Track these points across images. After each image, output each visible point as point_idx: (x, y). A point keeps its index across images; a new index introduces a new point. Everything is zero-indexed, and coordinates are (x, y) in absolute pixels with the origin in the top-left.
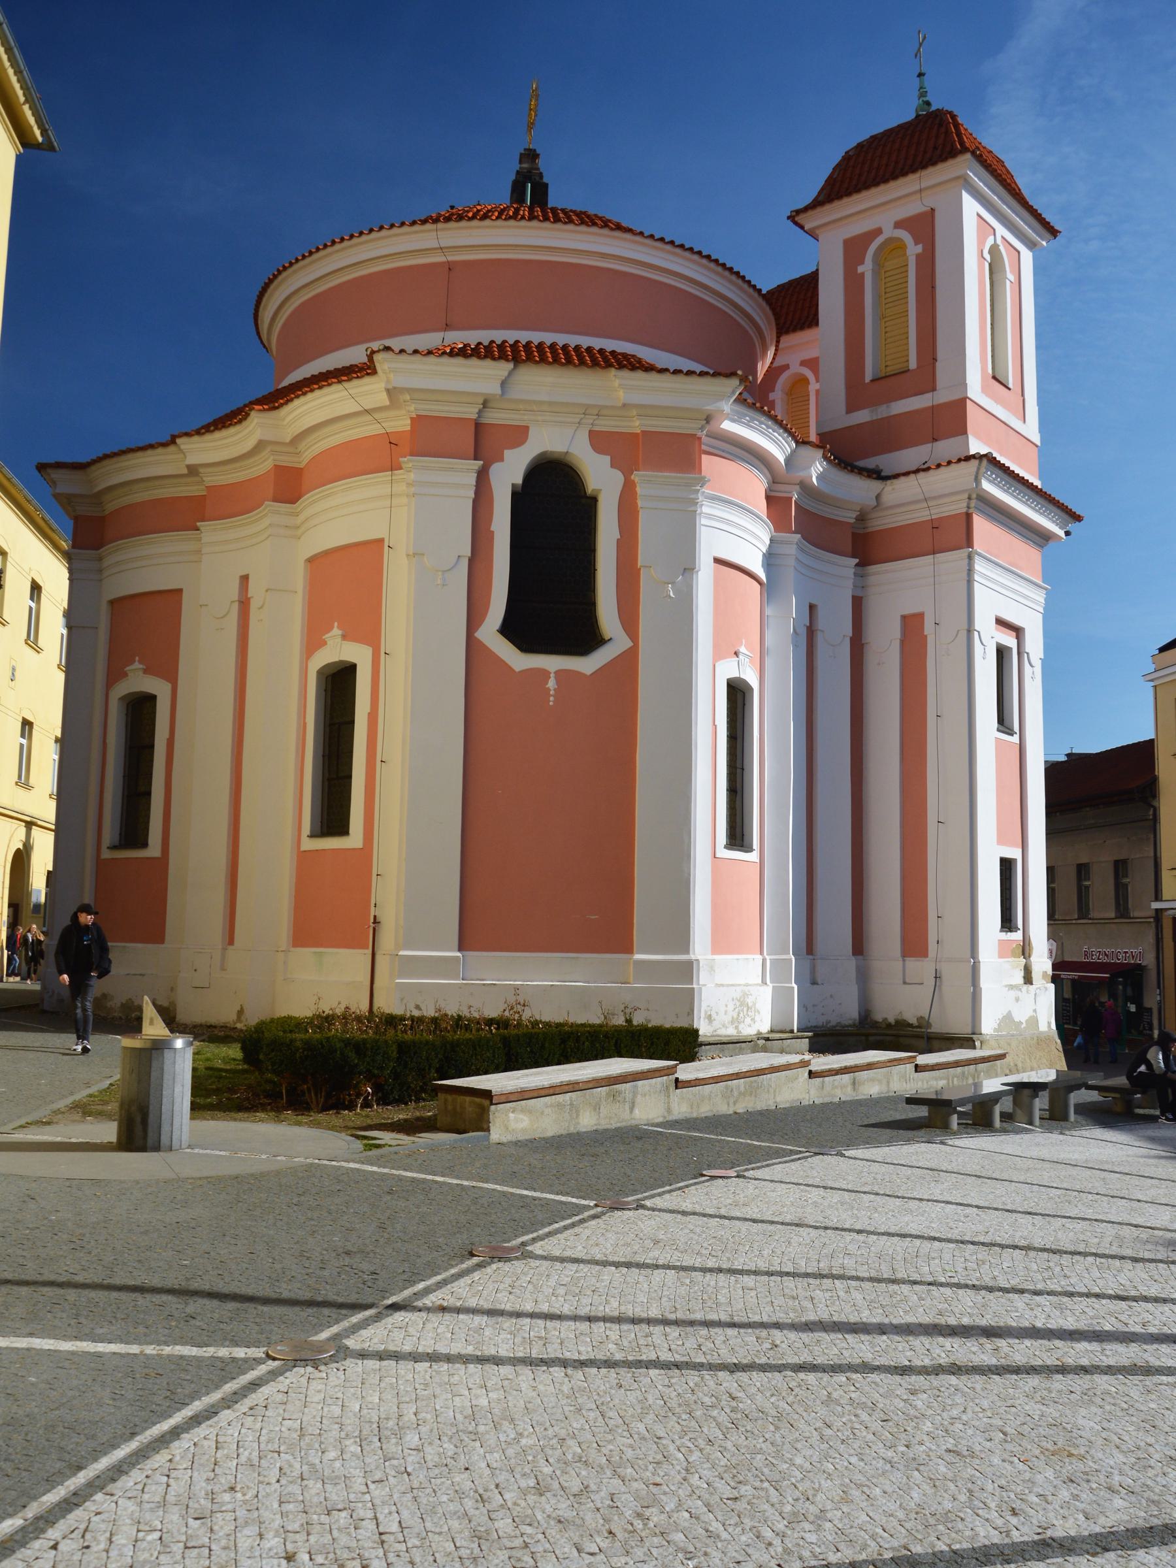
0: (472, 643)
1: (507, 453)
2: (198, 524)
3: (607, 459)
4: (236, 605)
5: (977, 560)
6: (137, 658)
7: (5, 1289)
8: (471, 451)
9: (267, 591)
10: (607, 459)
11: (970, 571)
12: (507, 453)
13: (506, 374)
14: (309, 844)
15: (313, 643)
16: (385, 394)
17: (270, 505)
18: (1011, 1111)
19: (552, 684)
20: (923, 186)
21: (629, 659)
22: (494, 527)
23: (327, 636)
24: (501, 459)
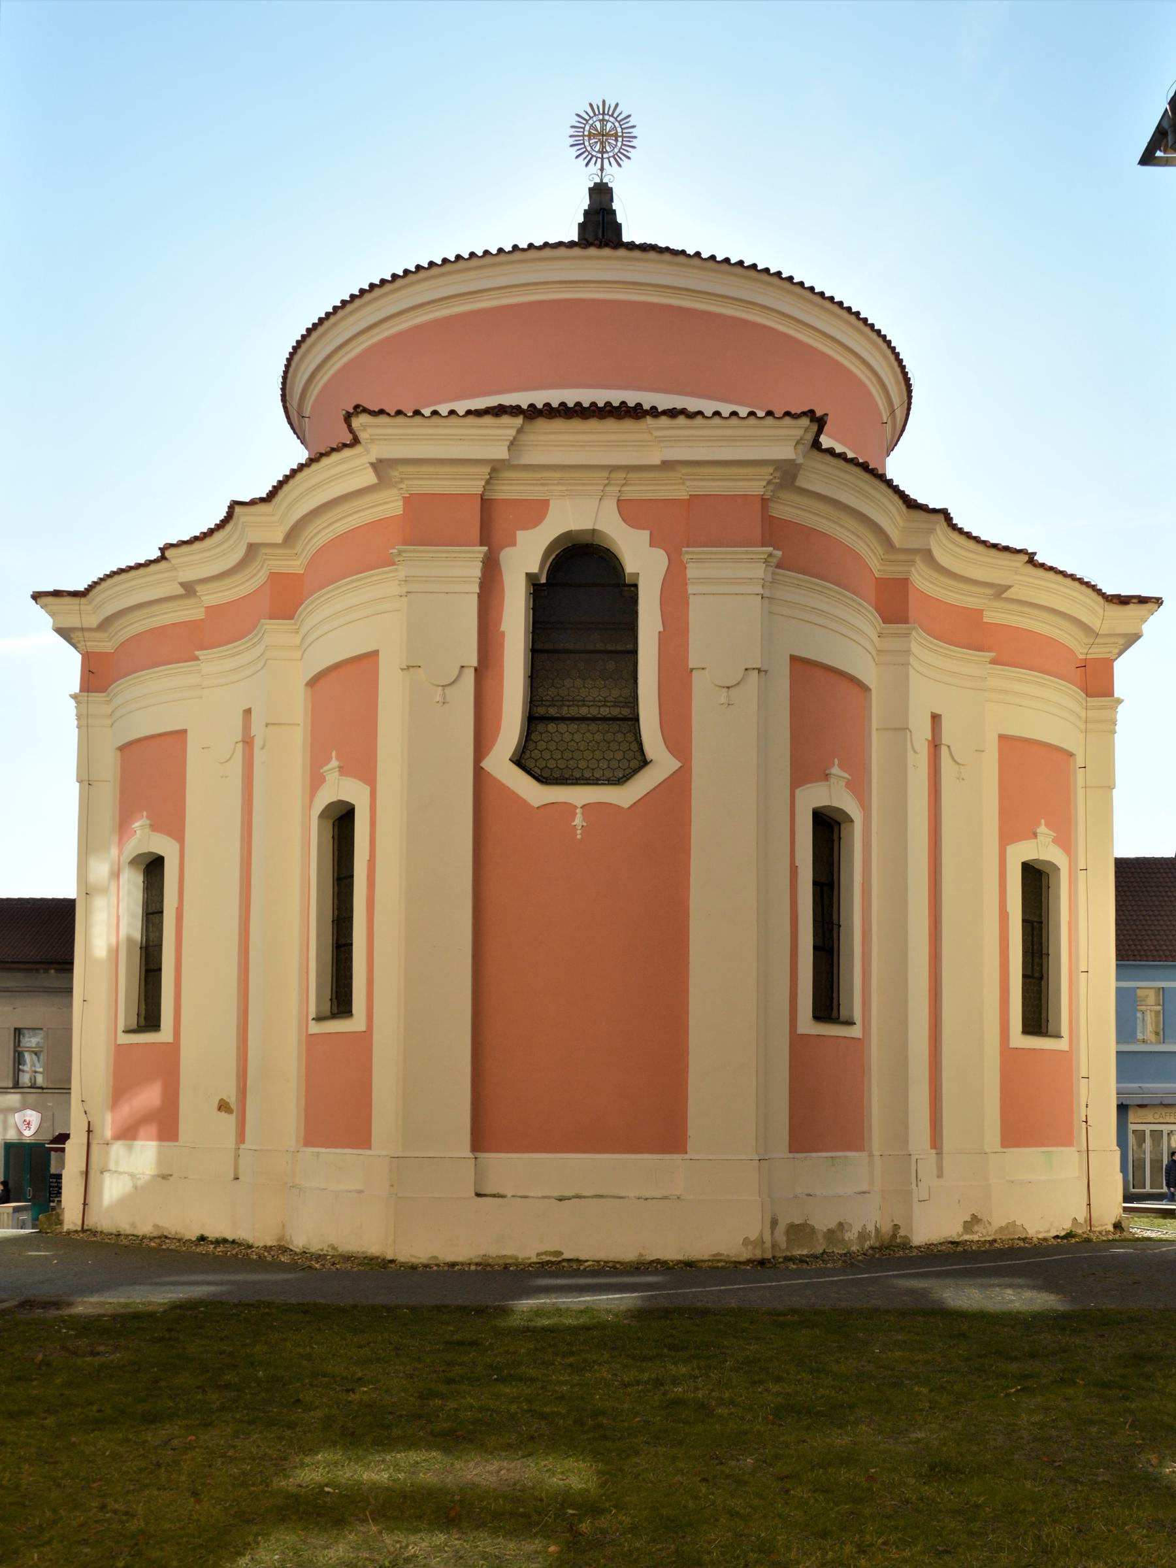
0: (479, 774)
1: (521, 535)
2: (197, 653)
3: (645, 534)
4: (240, 745)
8: (476, 534)
9: (267, 725)
10: (645, 534)
12: (521, 535)
13: (513, 432)
14: (315, 1028)
15: (316, 781)
16: (370, 470)
17: (269, 625)
18: (507, 457)
19: (578, 821)
21: (678, 784)
22: (504, 627)
23: (325, 769)
24: (513, 543)
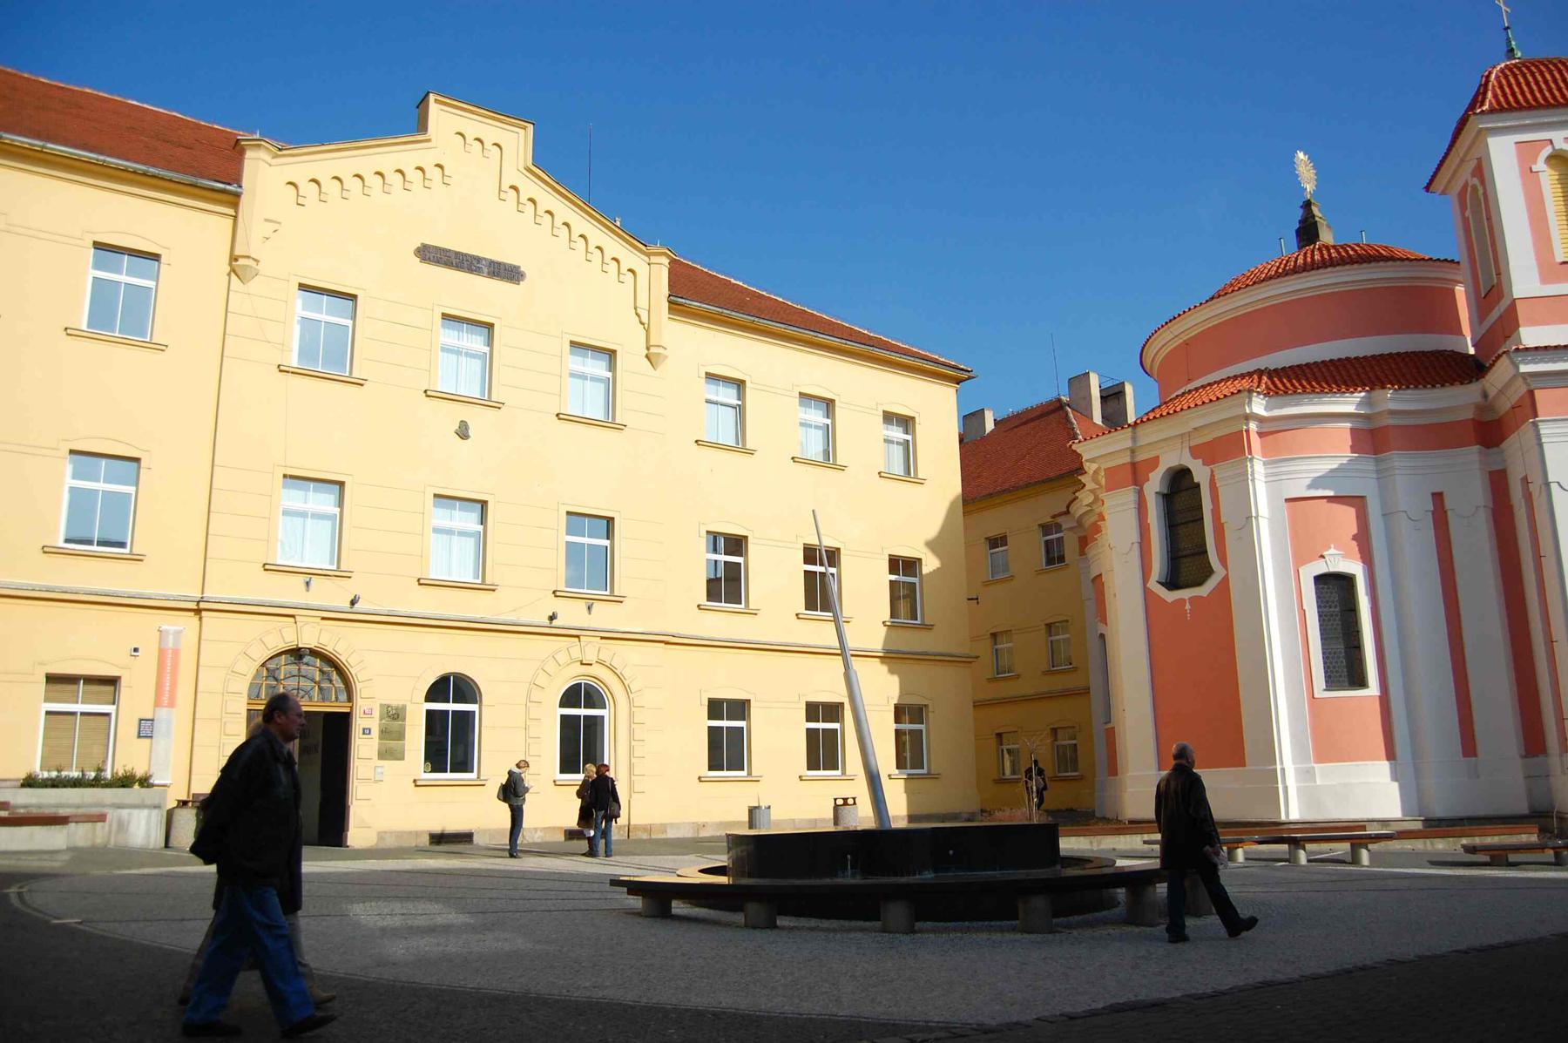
0: (1147, 593)
3: (1200, 461)
5: (1541, 426)
6: (1332, 546)
7: (3, 790)
10: (1200, 461)
11: (1538, 436)
12: (1150, 475)
19: (1188, 607)
20: (1461, 155)
21: (1226, 580)
